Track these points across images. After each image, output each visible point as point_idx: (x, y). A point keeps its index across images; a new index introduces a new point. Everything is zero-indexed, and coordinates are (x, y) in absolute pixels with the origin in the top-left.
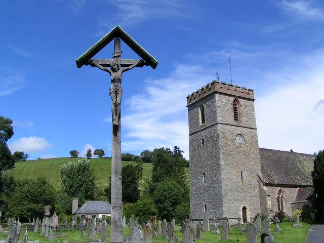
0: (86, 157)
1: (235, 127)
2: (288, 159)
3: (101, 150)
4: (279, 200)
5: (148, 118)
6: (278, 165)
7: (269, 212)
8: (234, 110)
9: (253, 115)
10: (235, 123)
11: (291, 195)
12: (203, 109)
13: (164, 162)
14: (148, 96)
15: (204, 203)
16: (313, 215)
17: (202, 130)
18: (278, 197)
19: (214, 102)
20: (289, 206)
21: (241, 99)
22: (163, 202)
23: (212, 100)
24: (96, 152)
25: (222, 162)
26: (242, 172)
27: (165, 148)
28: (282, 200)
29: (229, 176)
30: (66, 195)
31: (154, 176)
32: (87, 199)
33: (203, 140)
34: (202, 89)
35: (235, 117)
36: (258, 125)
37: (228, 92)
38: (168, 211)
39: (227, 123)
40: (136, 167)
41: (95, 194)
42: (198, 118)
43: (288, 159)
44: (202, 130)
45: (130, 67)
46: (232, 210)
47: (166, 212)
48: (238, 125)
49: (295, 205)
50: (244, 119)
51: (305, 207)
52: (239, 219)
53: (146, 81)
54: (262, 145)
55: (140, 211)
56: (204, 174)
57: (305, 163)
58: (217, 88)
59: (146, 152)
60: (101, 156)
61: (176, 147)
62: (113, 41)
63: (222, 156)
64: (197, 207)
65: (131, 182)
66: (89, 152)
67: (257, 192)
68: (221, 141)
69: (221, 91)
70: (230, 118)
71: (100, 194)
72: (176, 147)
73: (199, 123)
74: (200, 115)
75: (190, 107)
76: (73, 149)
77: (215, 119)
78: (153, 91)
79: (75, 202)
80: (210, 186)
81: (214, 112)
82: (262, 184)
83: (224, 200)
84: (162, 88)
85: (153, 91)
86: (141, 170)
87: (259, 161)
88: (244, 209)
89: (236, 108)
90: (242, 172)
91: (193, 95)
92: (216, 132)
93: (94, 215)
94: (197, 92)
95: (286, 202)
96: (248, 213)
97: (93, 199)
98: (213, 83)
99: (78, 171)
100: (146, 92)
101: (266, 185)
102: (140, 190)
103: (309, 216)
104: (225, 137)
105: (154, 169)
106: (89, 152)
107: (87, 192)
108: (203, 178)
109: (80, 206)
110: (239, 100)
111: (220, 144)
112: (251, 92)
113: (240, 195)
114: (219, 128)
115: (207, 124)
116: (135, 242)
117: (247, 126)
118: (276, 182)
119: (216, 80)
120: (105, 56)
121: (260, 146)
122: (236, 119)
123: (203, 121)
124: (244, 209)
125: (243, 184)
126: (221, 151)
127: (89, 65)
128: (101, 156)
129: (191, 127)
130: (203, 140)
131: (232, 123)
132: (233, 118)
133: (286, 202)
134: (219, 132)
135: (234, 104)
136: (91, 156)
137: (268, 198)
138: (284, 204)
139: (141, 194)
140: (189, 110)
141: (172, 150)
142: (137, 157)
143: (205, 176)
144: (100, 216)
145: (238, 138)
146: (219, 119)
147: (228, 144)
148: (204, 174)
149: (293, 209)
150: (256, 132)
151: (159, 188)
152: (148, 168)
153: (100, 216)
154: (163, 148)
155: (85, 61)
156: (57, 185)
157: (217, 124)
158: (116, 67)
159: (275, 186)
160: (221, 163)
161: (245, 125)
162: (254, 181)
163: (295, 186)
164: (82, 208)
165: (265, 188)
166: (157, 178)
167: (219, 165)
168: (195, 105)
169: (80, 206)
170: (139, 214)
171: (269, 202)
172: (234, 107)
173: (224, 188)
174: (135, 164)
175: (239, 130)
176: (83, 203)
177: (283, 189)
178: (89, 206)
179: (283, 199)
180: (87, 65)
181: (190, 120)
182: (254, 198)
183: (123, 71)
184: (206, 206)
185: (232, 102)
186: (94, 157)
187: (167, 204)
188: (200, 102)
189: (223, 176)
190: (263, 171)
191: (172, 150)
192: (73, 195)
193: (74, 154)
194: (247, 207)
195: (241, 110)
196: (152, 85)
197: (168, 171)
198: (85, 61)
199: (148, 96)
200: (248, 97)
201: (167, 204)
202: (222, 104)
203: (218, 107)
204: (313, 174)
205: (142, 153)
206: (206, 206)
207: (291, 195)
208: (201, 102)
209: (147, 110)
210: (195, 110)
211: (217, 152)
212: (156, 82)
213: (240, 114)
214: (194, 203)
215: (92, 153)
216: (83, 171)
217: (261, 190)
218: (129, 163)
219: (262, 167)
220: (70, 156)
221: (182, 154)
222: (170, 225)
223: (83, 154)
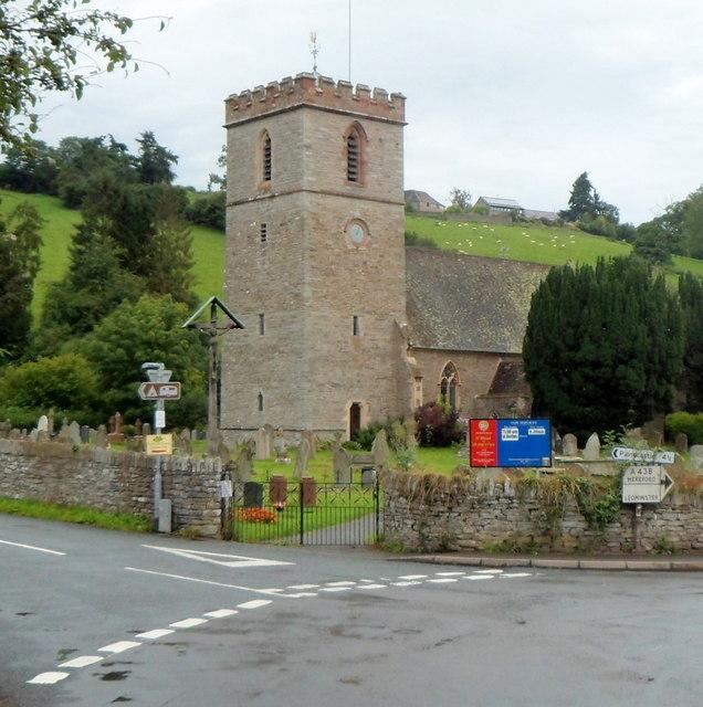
10: (347, 189)
50: (372, 176)
70: (336, 175)
77: (298, 176)
88: (355, 410)
101: (414, 350)
104: (320, 227)
110: (365, 124)
118: (441, 345)
124: (355, 410)
137: (416, 384)
139: (35, 326)
141: (135, 150)
146: (308, 180)
147: (327, 247)
161: (373, 195)
165: (411, 360)
175: (358, 209)
177: (459, 362)
190: (411, 311)
191: (135, 150)
195: (370, 152)
203: (308, 147)
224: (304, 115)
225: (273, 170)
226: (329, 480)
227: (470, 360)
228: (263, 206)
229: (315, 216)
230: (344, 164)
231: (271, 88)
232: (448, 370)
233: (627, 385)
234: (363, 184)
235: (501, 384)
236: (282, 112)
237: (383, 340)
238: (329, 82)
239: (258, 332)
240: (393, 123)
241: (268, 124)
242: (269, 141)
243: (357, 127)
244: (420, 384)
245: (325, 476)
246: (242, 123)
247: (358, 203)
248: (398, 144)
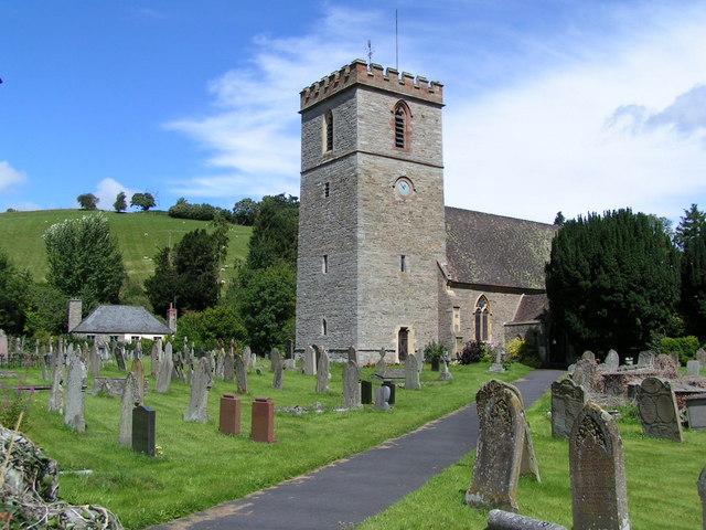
0: (113, 209)
1: (396, 162)
2: (511, 234)
3: (148, 196)
4: (480, 319)
5: (258, 125)
6: (480, 242)
7: (454, 340)
8: (397, 125)
9: (438, 137)
10: (396, 153)
11: (506, 307)
12: (331, 119)
13: (274, 225)
14: (260, 76)
15: (323, 317)
16: (543, 350)
17: (327, 164)
18: (478, 311)
19: (353, 107)
20: (500, 330)
21: (413, 102)
22: (257, 313)
23: (349, 102)
24: (137, 199)
25: (360, 234)
26: (403, 257)
27: (287, 196)
28: (485, 318)
29: (373, 262)
30: (56, 292)
31: (252, 256)
32: (102, 301)
33: (327, 185)
34: (332, 78)
35: (397, 140)
36: (449, 158)
37: (386, 87)
38: (267, 330)
40: (215, 235)
41: (121, 294)
42: (320, 139)
43: (511, 234)
44: (327, 164)
46: (375, 338)
47: (263, 333)
48: (402, 157)
49: (512, 328)
50: (416, 146)
51: (532, 334)
53: (256, 40)
54: (451, 201)
55: (211, 329)
56: (325, 257)
58: (361, 77)
59: (246, 202)
60: (146, 208)
63: (361, 222)
64: (308, 326)
65: (202, 267)
66: (121, 198)
67: (433, 299)
68: (363, 190)
69: (369, 82)
70: (386, 142)
71: (135, 291)
73: (320, 148)
74: (325, 131)
75: (307, 113)
77: (353, 142)
78: (271, 64)
79: (75, 307)
80: (336, 283)
81: (352, 128)
82: (445, 283)
83: (359, 312)
84: (292, 58)
85: (271, 64)
86: (225, 241)
88: (404, 332)
89: (401, 121)
90: (403, 257)
91: (313, 88)
92: (352, 171)
93: (115, 335)
94: (322, 83)
95: (494, 322)
97: (115, 301)
98: (354, 65)
99: (83, 242)
100: (255, 67)
101: (453, 285)
102: (221, 284)
103: (536, 353)
104: (372, 182)
105: (254, 242)
106: (121, 198)
107: (101, 286)
108: (324, 265)
109: (85, 315)
110: (409, 103)
111: (359, 195)
112: (437, 89)
113: (388, 302)
114: (360, 162)
115: (338, 152)
116: (527, 520)
117: (422, 160)
118: (475, 281)
119: (362, 56)
121: (449, 202)
122: (399, 143)
123: (330, 147)
124: (404, 332)
125: (404, 282)
126: (360, 210)
128: (146, 208)
129: (305, 154)
130: (327, 185)
131: (390, 153)
132: (393, 141)
133: (495, 321)
134: (359, 171)
135: (397, 113)
136: (124, 207)
137: (455, 312)
138: (490, 326)
139: (223, 293)
140: (303, 120)
143: (326, 262)
144: (128, 337)
145: (399, 185)
146: (361, 143)
147: (378, 198)
148: (325, 257)
149: (508, 336)
151: (230, 285)
152: (240, 236)
154: (282, 195)
157: (355, 153)
159: (461, 288)
160: (359, 236)
161: (417, 159)
162: (428, 276)
163: (517, 291)
164: (89, 320)
165: (450, 292)
166: (257, 261)
167: (354, 240)
168: (317, 110)
169: (85, 315)
170: (208, 336)
171: (456, 321)
172: (397, 120)
173: (361, 287)
174: (209, 228)
175: (404, 168)
176: (93, 308)
177: (490, 295)
178: (105, 315)
179: (489, 316)
181: (305, 142)
182: (427, 311)
184: (325, 323)
185: (392, 107)
186: (130, 209)
187: (266, 316)
188: (326, 102)
189: (361, 263)
190: (450, 252)
192: (72, 291)
193: (88, 202)
194: (410, 328)
195: (412, 125)
196: (270, 51)
197: (283, 246)
199: (260, 76)
200: (430, 98)
201: (266, 316)
202: (370, 111)
204: (548, 268)
205: (237, 205)
206: (325, 323)
207: (506, 307)
208: (328, 105)
209: (257, 108)
210: (315, 120)
211: (353, 212)
212: (281, 44)
213: (408, 133)
214: (303, 317)
215: (128, 200)
216: (94, 241)
217: (443, 296)
218: (204, 225)
220: (78, 206)
223: (106, 203)
224: (360, 94)
225: (335, 139)
229: (368, 173)
230: (393, 132)
233: (636, 308)
234: (408, 150)
244: (458, 312)
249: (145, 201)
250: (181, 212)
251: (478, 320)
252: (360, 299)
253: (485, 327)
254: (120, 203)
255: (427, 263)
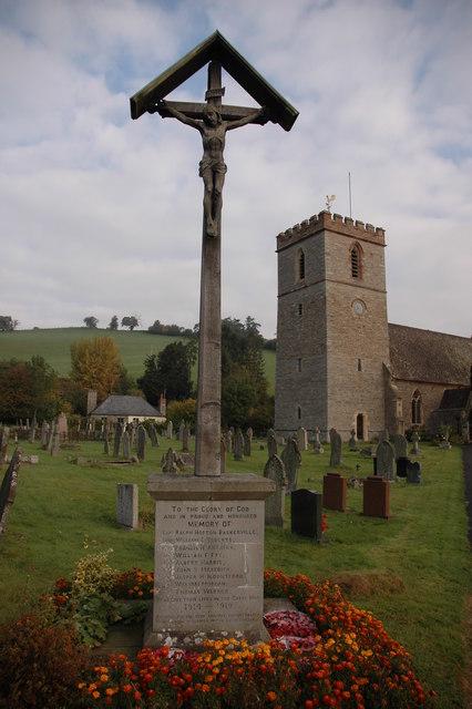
6: (416, 348)
10: (353, 280)
19: (321, 245)
29: (338, 363)
39: (340, 280)
45: (241, 122)
50: (367, 275)
52: (353, 433)
54: (391, 320)
57: (458, 351)
60: (132, 327)
61: (249, 318)
62: (206, 67)
63: (329, 333)
66: (115, 319)
68: (330, 309)
70: (347, 275)
72: (249, 318)
76: (89, 316)
81: (322, 263)
87: (388, 343)
96: (366, 424)
104: (336, 302)
106: (115, 319)
109: (99, 402)
110: (362, 243)
116: (467, 685)
118: (412, 378)
120: (190, 92)
123: (302, 276)
124: (360, 418)
127: (157, 114)
128: (132, 327)
141: (243, 322)
142: (188, 331)
146: (329, 273)
150: (385, 298)
153: (131, 419)
155: (140, 106)
156: (61, 367)
158: (214, 117)
161: (368, 286)
167: (324, 346)
169: (99, 402)
171: (399, 409)
173: (330, 382)
175: (359, 293)
180: (152, 112)
183: (228, 129)
194: (365, 414)
195: (365, 260)
198: (140, 106)
203: (329, 254)
211: (323, 327)
215: (119, 321)
219: (392, 354)
220: (84, 325)
221: (258, 328)
222: (247, 437)
225: (306, 271)
226: (265, 444)
227: (430, 387)
228: (300, 294)
230: (350, 266)
231: (304, 224)
232: (416, 394)
235: (449, 399)
236: (312, 235)
237: (377, 374)
238: (340, 217)
239: (298, 276)
240: (379, 244)
241: (301, 245)
242: (303, 255)
243: (357, 245)
245: (262, 448)
246: (290, 246)
247: (360, 290)
248: (382, 257)
249: (130, 322)
250: (157, 330)
251: (413, 408)
252: (329, 391)
253: (419, 412)
254: (114, 323)
255: (377, 365)
